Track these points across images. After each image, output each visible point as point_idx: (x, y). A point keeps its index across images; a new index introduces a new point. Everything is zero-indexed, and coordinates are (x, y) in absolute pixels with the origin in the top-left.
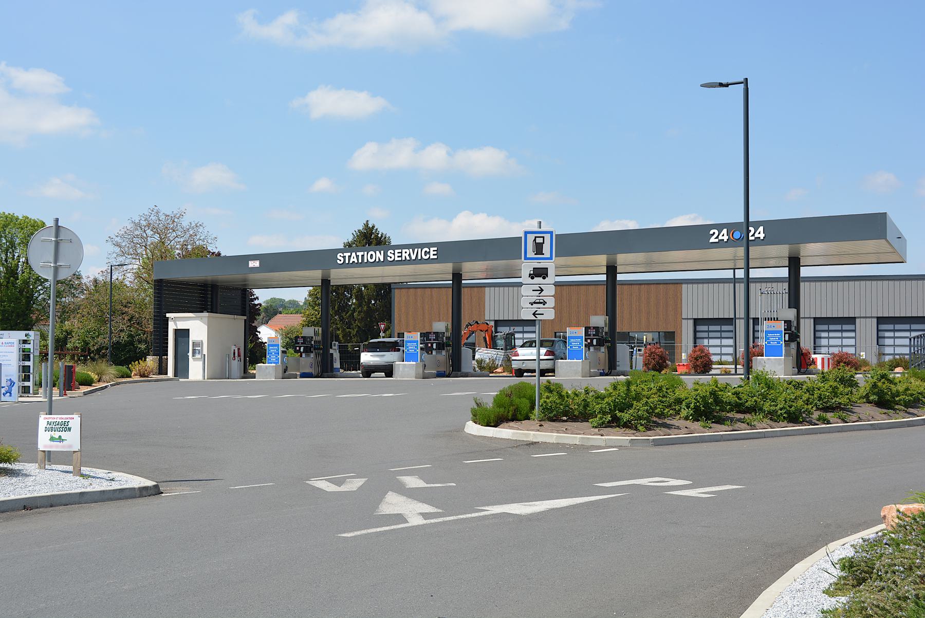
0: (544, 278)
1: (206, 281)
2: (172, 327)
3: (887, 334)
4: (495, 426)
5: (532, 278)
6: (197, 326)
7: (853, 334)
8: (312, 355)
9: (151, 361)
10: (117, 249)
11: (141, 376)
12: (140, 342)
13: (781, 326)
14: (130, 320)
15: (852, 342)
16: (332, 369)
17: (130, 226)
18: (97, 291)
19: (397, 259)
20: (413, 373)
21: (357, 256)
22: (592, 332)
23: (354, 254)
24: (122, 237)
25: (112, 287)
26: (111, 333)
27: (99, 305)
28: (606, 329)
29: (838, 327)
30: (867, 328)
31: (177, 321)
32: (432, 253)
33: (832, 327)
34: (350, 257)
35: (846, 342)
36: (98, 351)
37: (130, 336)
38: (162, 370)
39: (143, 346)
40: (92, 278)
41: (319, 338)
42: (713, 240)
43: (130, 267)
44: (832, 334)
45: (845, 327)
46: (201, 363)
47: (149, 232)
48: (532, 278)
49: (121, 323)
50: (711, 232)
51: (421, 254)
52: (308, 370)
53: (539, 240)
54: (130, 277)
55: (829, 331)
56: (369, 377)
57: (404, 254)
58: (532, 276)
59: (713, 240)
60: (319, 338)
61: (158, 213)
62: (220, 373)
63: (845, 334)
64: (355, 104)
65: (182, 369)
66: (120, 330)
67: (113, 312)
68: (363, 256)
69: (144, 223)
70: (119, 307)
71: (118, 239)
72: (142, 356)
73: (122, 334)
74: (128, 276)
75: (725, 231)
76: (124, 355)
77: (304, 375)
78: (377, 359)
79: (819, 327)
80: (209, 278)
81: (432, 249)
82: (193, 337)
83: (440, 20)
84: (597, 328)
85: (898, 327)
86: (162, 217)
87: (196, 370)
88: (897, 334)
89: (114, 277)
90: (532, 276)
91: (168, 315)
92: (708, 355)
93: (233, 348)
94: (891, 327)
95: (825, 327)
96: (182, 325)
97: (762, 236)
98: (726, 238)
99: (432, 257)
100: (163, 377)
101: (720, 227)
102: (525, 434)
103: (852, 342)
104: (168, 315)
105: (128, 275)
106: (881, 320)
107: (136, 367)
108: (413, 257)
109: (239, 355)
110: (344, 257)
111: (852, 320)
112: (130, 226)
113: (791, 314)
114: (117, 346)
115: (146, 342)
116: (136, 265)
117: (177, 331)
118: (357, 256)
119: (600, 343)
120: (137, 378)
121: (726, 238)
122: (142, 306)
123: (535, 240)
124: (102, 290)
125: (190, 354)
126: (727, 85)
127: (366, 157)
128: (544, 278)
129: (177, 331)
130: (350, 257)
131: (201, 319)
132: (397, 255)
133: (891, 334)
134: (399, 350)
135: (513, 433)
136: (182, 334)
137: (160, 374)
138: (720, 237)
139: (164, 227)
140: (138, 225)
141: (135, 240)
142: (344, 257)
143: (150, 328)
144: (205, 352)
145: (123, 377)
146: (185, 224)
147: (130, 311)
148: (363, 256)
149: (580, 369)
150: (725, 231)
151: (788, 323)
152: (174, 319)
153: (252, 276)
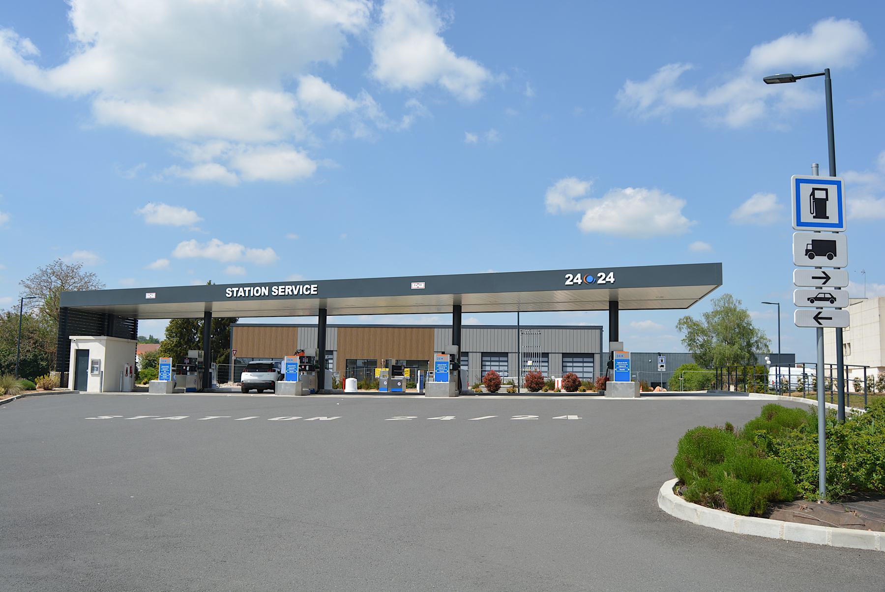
0: (830, 258)
1: (104, 310)
2: (73, 347)
3: (569, 364)
4: (766, 515)
5: (811, 257)
6: (97, 348)
7: (592, 365)
8: (196, 374)
9: (54, 376)
10: (27, 290)
11: (45, 389)
12: (42, 360)
13: (448, 358)
14: (34, 343)
15: (506, 368)
16: (211, 385)
17: (38, 273)
18: (9, 321)
19: (280, 294)
20: (294, 390)
21: (245, 291)
22: (306, 360)
23: (241, 289)
24: (32, 280)
25: (22, 318)
26: (19, 352)
27: (11, 332)
28: (317, 358)
29: (497, 359)
30: (556, 360)
31: (78, 343)
32: (312, 289)
33: (493, 359)
34: (237, 291)
35: (586, 369)
36: (8, 366)
37: (35, 356)
38: (64, 383)
39: (44, 364)
40: (6, 311)
41: (202, 360)
42: (568, 283)
43: (37, 303)
44: (493, 363)
45: (501, 359)
46: (99, 378)
47: (53, 278)
48: (811, 257)
49: (27, 345)
50: (567, 276)
51: (303, 290)
52: (192, 386)
53: (820, 195)
54: (37, 310)
55: (491, 361)
56: (247, 392)
57: (287, 290)
58: (810, 254)
59: (568, 283)
60: (202, 360)
61: (61, 264)
62: (114, 386)
63: (501, 364)
64: (181, 216)
65: (81, 383)
66: (27, 350)
67: (21, 336)
68: (249, 291)
69: (50, 271)
70: (26, 333)
71: (29, 283)
72: (45, 372)
73: (28, 354)
74: (34, 310)
75: (579, 276)
76: (30, 371)
77: (189, 390)
78: (256, 378)
79: (484, 359)
80: (107, 307)
81: (313, 286)
82: (92, 356)
83: (238, 172)
84: (309, 358)
85: (575, 360)
86: (64, 268)
87: (94, 384)
88: (575, 364)
89: (24, 310)
90: (810, 254)
91: (71, 337)
92: (498, 377)
93: (126, 366)
94: (571, 360)
95: (488, 359)
96: (82, 346)
97: (612, 280)
98: (579, 281)
99: (312, 293)
100: (63, 390)
101: (574, 272)
102: (861, 537)
103: (506, 368)
104: (71, 337)
105: (35, 310)
106: (565, 355)
107: (41, 381)
108: (296, 293)
109: (131, 372)
110: (233, 291)
111: (506, 354)
112: (38, 273)
113: (454, 349)
114: (24, 363)
115: (47, 360)
116: (42, 303)
117: (78, 352)
118: (245, 291)
119: (312, 369)
120: (41, 391)
121: (579, 281)
122: (44, 334)
123: (813, 194)
124: (14, 322)
125: (89, 370)
126: (793, 79)
127: (187, 249)
128: (830, 258)
129: (78, 352)
130: (237, 291)
131: (100, 341)
132: (280, 290)
133: (571, 364)
134: (274, 371)
135: (834, 535)
136: (83, 354)
137: (61, 386)
138: (575, 281)
139: (65, 276)
140: (44, 273)
141: (42, 284)
142: (233, 291)
143: (53, 349)
144: (103, 369)
145: (28, 389)
146: (82, 273)
147: (36, 337)
148: (249, 291)
149: (448, 389)
150: (579, 276)
151: (452, 356)
152: (77, 341)
153: (142, 307)
